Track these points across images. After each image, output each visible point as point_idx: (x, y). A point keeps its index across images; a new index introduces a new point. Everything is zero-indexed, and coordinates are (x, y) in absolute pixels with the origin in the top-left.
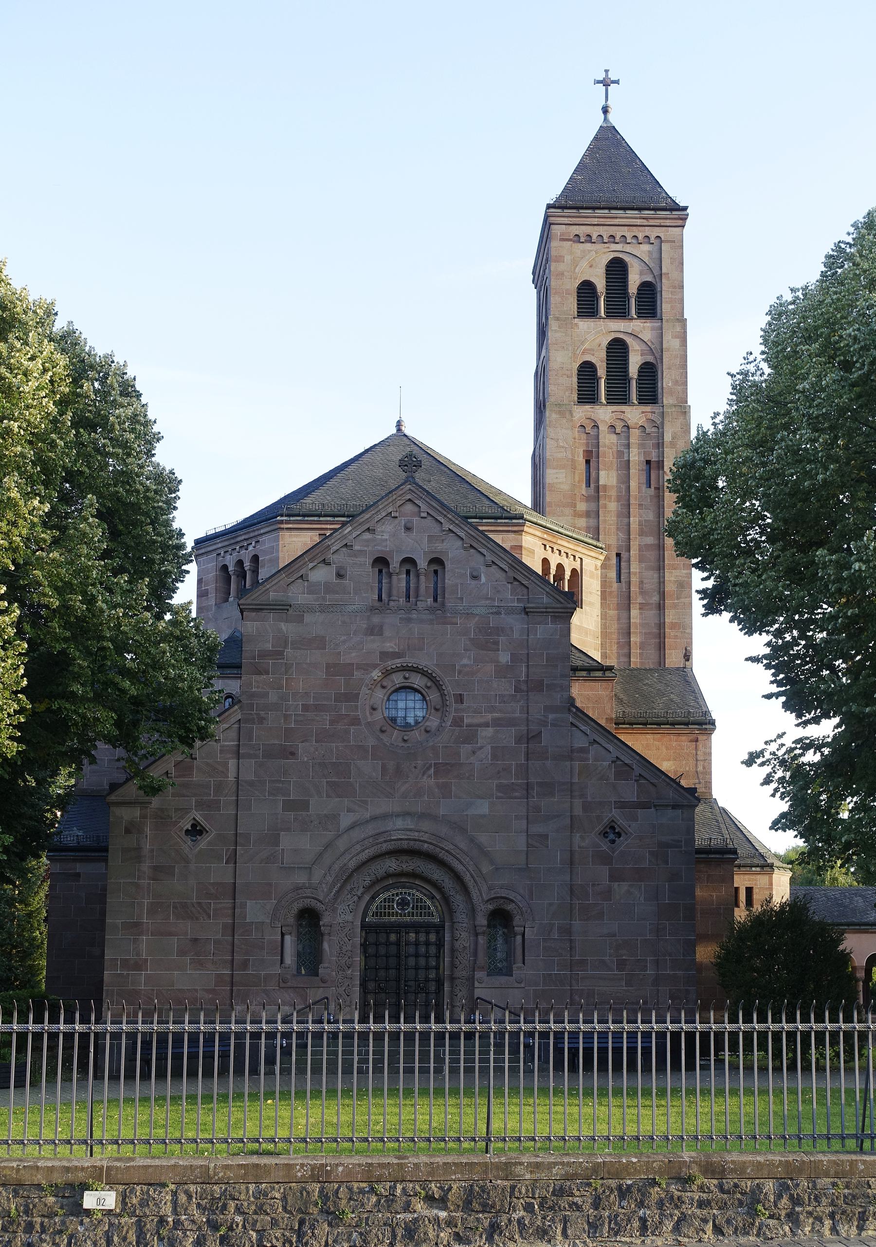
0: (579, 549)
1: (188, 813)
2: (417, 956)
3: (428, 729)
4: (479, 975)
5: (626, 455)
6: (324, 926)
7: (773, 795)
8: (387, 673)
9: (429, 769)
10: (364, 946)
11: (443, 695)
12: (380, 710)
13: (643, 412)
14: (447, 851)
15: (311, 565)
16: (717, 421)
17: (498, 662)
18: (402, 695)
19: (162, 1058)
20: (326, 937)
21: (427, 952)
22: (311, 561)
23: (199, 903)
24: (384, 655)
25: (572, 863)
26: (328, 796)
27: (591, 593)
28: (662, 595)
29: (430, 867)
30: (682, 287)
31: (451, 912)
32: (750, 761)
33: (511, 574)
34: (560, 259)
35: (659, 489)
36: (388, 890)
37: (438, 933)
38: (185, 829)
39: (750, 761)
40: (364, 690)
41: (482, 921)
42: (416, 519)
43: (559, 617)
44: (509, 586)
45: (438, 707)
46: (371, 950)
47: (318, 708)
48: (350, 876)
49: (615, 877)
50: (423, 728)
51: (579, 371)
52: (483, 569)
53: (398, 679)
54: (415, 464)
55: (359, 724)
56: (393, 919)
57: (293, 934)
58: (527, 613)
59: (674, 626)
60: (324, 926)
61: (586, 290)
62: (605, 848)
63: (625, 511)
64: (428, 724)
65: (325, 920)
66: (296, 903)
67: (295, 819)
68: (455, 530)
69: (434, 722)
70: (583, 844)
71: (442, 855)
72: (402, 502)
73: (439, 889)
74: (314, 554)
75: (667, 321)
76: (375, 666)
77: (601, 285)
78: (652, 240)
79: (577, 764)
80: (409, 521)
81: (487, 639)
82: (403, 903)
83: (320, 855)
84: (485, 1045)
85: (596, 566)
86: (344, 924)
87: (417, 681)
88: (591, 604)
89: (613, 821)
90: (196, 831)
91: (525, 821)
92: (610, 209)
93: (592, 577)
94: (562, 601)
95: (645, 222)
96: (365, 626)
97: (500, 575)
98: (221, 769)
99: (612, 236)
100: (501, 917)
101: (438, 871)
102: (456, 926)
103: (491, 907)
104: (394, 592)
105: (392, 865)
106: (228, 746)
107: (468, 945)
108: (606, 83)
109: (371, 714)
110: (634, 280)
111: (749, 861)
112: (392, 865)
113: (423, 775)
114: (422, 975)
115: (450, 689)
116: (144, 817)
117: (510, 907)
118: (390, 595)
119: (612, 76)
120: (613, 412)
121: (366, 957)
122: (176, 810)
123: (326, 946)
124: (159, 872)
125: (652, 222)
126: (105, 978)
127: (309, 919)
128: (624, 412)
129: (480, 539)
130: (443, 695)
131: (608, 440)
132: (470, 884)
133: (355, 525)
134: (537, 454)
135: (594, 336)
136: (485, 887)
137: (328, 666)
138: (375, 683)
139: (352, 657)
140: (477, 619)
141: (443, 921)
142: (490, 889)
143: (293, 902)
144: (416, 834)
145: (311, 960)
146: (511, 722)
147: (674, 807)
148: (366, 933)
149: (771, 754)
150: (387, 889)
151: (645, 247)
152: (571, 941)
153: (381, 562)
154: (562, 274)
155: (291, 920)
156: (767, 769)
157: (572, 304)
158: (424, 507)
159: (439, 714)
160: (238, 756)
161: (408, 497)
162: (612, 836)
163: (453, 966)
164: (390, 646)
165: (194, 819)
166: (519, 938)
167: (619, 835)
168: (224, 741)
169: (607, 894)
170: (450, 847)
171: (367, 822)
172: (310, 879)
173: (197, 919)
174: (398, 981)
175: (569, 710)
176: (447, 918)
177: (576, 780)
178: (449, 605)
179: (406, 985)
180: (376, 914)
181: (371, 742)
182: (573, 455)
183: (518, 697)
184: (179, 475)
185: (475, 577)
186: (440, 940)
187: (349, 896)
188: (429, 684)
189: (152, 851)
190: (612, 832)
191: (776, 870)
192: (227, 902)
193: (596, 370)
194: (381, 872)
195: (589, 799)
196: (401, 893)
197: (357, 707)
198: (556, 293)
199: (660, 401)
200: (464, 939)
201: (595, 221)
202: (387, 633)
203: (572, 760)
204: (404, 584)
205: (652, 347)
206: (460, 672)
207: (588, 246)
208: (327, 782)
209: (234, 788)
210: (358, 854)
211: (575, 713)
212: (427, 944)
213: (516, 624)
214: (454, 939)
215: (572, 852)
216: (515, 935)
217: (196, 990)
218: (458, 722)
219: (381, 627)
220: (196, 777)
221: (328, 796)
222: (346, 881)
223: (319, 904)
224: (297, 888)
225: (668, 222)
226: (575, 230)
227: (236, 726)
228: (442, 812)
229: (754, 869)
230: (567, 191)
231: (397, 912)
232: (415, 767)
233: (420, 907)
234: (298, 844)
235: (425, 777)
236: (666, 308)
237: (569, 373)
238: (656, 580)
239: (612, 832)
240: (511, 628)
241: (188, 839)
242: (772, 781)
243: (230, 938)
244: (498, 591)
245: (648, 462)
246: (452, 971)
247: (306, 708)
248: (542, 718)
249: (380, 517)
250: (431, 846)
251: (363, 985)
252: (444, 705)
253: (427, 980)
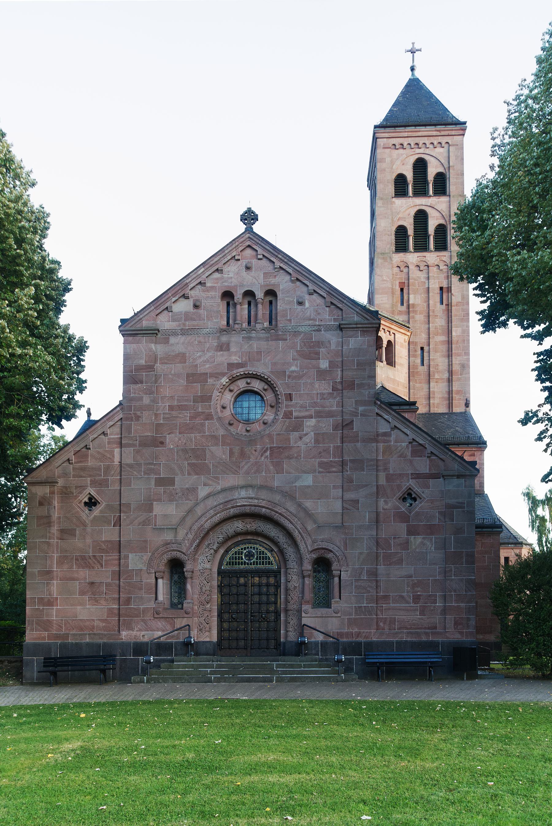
0: (393, 327)
1: (84, 489)
2: (260, 594)
3: (265, 421)
4: (304, 607)
5: (427, 284)
6: (187, 571)
7: (546, 451)
8: (233, 380)
9: (265, 452)
11: (276, 395)
12: (228, 408)
13: (438, 256)
14: (280, 514)
15: (174, 299)
16: (495, 135)
17: (319, 368)
18: (246, 397)
20: (189, 580)
21: (268, 591)
22: (174, 295)
23: (94, 556)
24: (231, 366)
25: (377, 521)
26: (189, 474)
27: (401, 357)
28: (451, 372)
29: (268, 527)
30: (463, 174)
31: (285, 561)
32: (524, 422)
33: (329, 299)
34: (383, 160)
35: (448, 305)
36: (238, 545)
37: (276, 577)
38: (83, 501)
39: (524, 422)
40: (216, 393)
41: (308, 566)
42: (254, 261)
43: (366, 331)
44: (327, 309)
45: (273, 404)
46: (225, 590)
47: (181, 408)
48: (207, 533)
49: (412, 531)
50: (261, 421)
51: (396, 232)
52: (307, 297)
53: (242, 384)
54: (253, 217)
55: (212, 419)
56: (242, 567)
57: (165, 578)
58: (341, 329)
59: (458, 392)
60: (187, 571)
61: (400, 180)
62: (403, 509)
63: (426, 320)
64: (265, 417)
65: (188, 567)
66: (165, 555)
67: (165, 492)
68: (284, 267)
69: (270, 417)
70: (386, 507)
71: (276, 517)
72: (243, 248)
73: (276, 543)
74: (176, 290)
75: (453, 196)
76: (223, 374)
77: (410, 176)
78: (443, 144)
79: (381, 445)
80: (248, 262)
81: (311, 351)
83: (183, 519)
85: (405, 340)
86: (204, 570)
87: (257, 385)
88: (401, 365)
89: (410, 489)
90: (91, 503)
91: (341, 490)
92: (415, 126)
93: (402, 346)
94: (369, 318)
95: (438, 133)
96: (216, 344)
97: (319, 300)
98: (108, 456)
99: (417, 144)
100: (323, 564)
101: (274, 530)
102: (289, 571)
103: (314, 556)
104: (238, 318)
105: (239, 525)
106: (114, 438)
107: (298, 585)
108: (413, 52)
109: (222, 412)
110: (432, 172)
111: (506, 541)
112: (239, 525)
113: (262, 456)
114: (264, 608)
115: (281, 390)
116: (52, 493)
117: (330, 556)
118: (235, 320)
119: (417, 47)
120: (418, 257)
121: (222, 595)
122: (76, 487)
123: (189, 587)
124: (66, 533)
125: (443, 133)
126: (27, 611)
127: (176, 567)
128: (425, 257)
129: (304, 273)
130: (276, 395)
131: (415, 273)
133: (207, 266)
134: (371, 291)
135: (405, 209)
136: (310, 540)
137: (188, 376)
138: (224, 387)
139: (207, 368)
140: (302, 336)
141: (279, 568)
142: (314, 542)
143: (163, 554)
144: (256, 501)
146: (330, 414)
147: (459, 477)
148: (222, 577)
149: (544, 414)
150: (237, 544)
151: (439, 150)
152: (377, 581)
153: (228, 295)
154: (384, 170)
155: (162, 568)
156: (541, 427)
157: (391, 189)
159: (274, 410)
160: (121, 445)
161: (248, 243)
162: (409, 501)
163: (287, 601)
164: (235, 359)
165: (90, 494)
166: (336, 580)
167: (415, 499)
168: (111, 434)
169: (406, 545)
170: (282, 511)
171: (219, 492)
172: (175, 537)
173: (93, 568)
174: (245, 612)
175: (375, 403)
176: (282, 566)
177: (380, 457)
178: (280, 325)
179: (252, 616)
181: (221, 432)
182: (392, 285)
183: (335, 394)
184: (47, 210)
185: (300, 303)
186: (277, 582)
187: (207, 550)
188: (266, 387)
189: (59, 518)
191: (524, 546)
192: (115, 556)
193: (407, 231)
195: (391, 472)
196: (248, 548)
197: (210, 406)
198: (380, 182)
199: (449, 249)
200: (295, 581)
201: (406, 134)
202: (233, 349)
203: (377, 442)
204: (246, 312)
205: (444, 214)
206: (289, 377)
207: (401, 151)
208: (188, 464)
209: (119, 469)
210: (212, 517)
211: (380, 405)
212: (268, 585)
213: (333, 339)
214: (287, 581)
215: (378, 514)
216: (334, 577)
217: (93, 620)
218: (288, 415)
220: (91, 463)
221: (189, 474)
222: (203, 538)
223: (183, 555)
224: (167, 544)
225: (453, 133)
227: (119, 423)
228: (276, 484)
229: (510, 545)
230: (386, 119)
231: (245, 562)
232: (255, 451)
233: (263, 558)
234: (166, 511)
235: (263, 458)
237: (389, 233)
238: (447, 364)
239: (409, 496)
240: (329, 342)
242: (545, 437)
243: (117, 582)
244: (319, 314)
245: (441, 289)
246: (286, 605)
247: (171, 408)
248: (354, 410)
249: (226, 260)
250: (268, 510)
251: (220, 616)
252: (278, 403)
253: (268, 612)
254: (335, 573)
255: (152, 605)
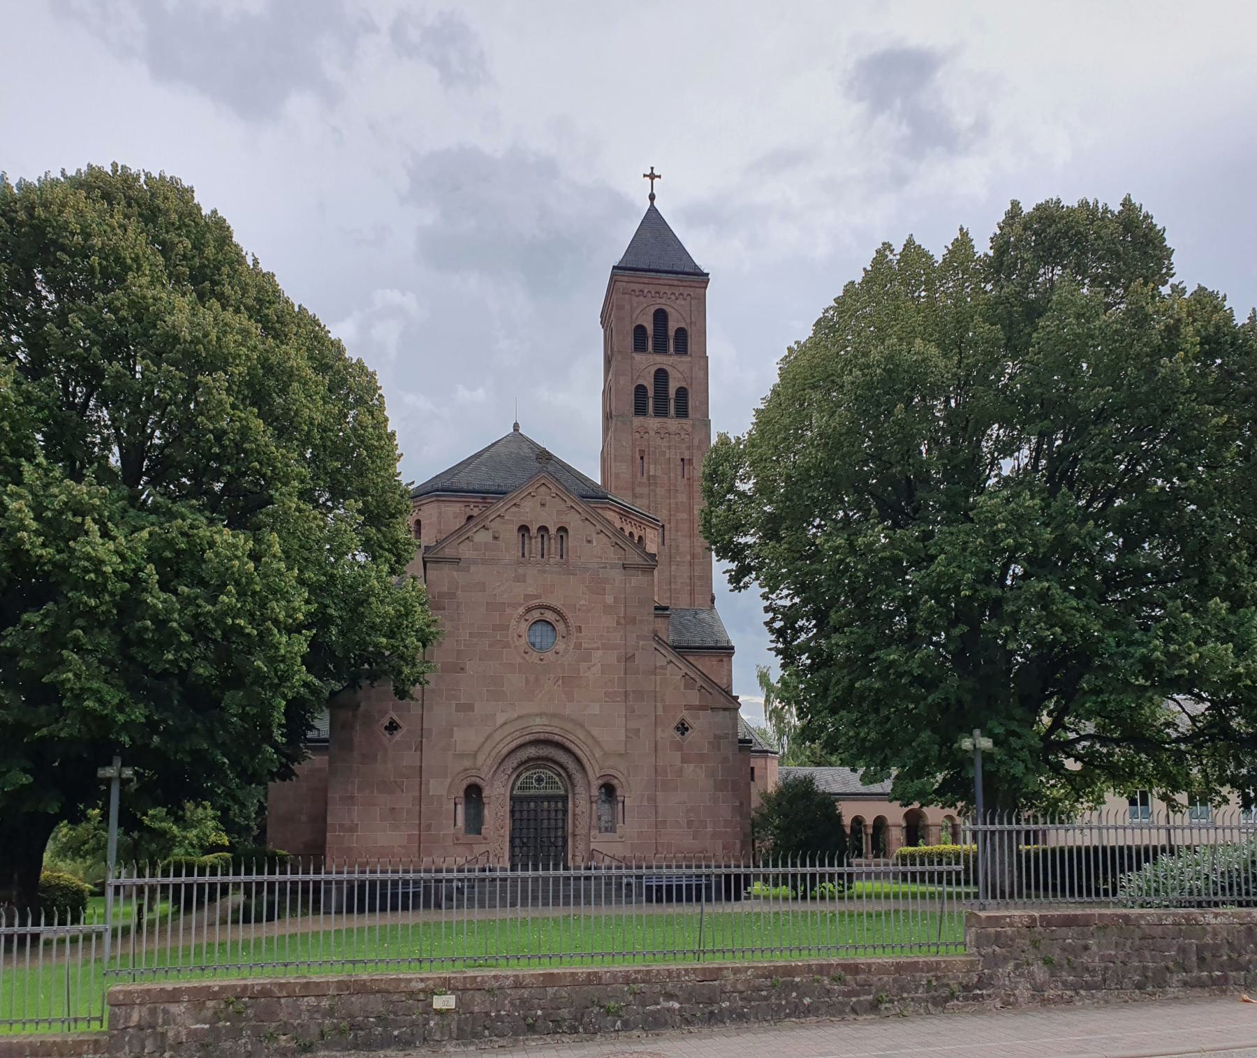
10: (512, 812)
11: (567, 627)
19: (372, 897)
31: (573, 786)
40: (513, 622)
52: (594, 535)
53: (536, 615)
71: (568, 744)
73: (565, 769)
76: (520, 605)
82: (539, 780)
84: (598, 885)
87: (549, 616)
97: (605, 539)
100: (609, 790)
105: (532, 752)
110: (672, 327)
112: (532, 752)
117: (615, 782)
119: (656, 172)
123: (486, 812)
127: (474, 794)
130: (567, 627)
132: (587, 766)
135: (647, 364)
145: (475, 824)
147: (725, 709)
150: (527, 769)
153: (524, 529)
155: (462, 794)
157: (630, 341)
158: (554, 490)
163: (575, 826)
170: (573, 738)
174: (535, 838)
180: (520, 788)
185: (589, 542)
190: (683, 728)
194: (524, 758)
213: (617, 575)
214: (575, 806)
218: (578, 646)
219: (524, 576)
226: (633, 286)
236: (692, 346)
241: (386, 733)
254: (620, 799)
255: (452, 830)
